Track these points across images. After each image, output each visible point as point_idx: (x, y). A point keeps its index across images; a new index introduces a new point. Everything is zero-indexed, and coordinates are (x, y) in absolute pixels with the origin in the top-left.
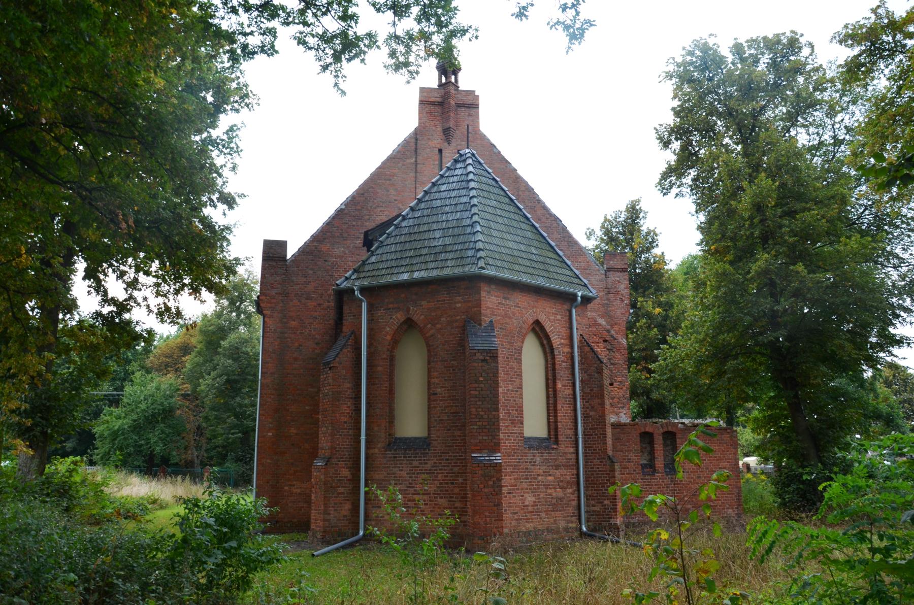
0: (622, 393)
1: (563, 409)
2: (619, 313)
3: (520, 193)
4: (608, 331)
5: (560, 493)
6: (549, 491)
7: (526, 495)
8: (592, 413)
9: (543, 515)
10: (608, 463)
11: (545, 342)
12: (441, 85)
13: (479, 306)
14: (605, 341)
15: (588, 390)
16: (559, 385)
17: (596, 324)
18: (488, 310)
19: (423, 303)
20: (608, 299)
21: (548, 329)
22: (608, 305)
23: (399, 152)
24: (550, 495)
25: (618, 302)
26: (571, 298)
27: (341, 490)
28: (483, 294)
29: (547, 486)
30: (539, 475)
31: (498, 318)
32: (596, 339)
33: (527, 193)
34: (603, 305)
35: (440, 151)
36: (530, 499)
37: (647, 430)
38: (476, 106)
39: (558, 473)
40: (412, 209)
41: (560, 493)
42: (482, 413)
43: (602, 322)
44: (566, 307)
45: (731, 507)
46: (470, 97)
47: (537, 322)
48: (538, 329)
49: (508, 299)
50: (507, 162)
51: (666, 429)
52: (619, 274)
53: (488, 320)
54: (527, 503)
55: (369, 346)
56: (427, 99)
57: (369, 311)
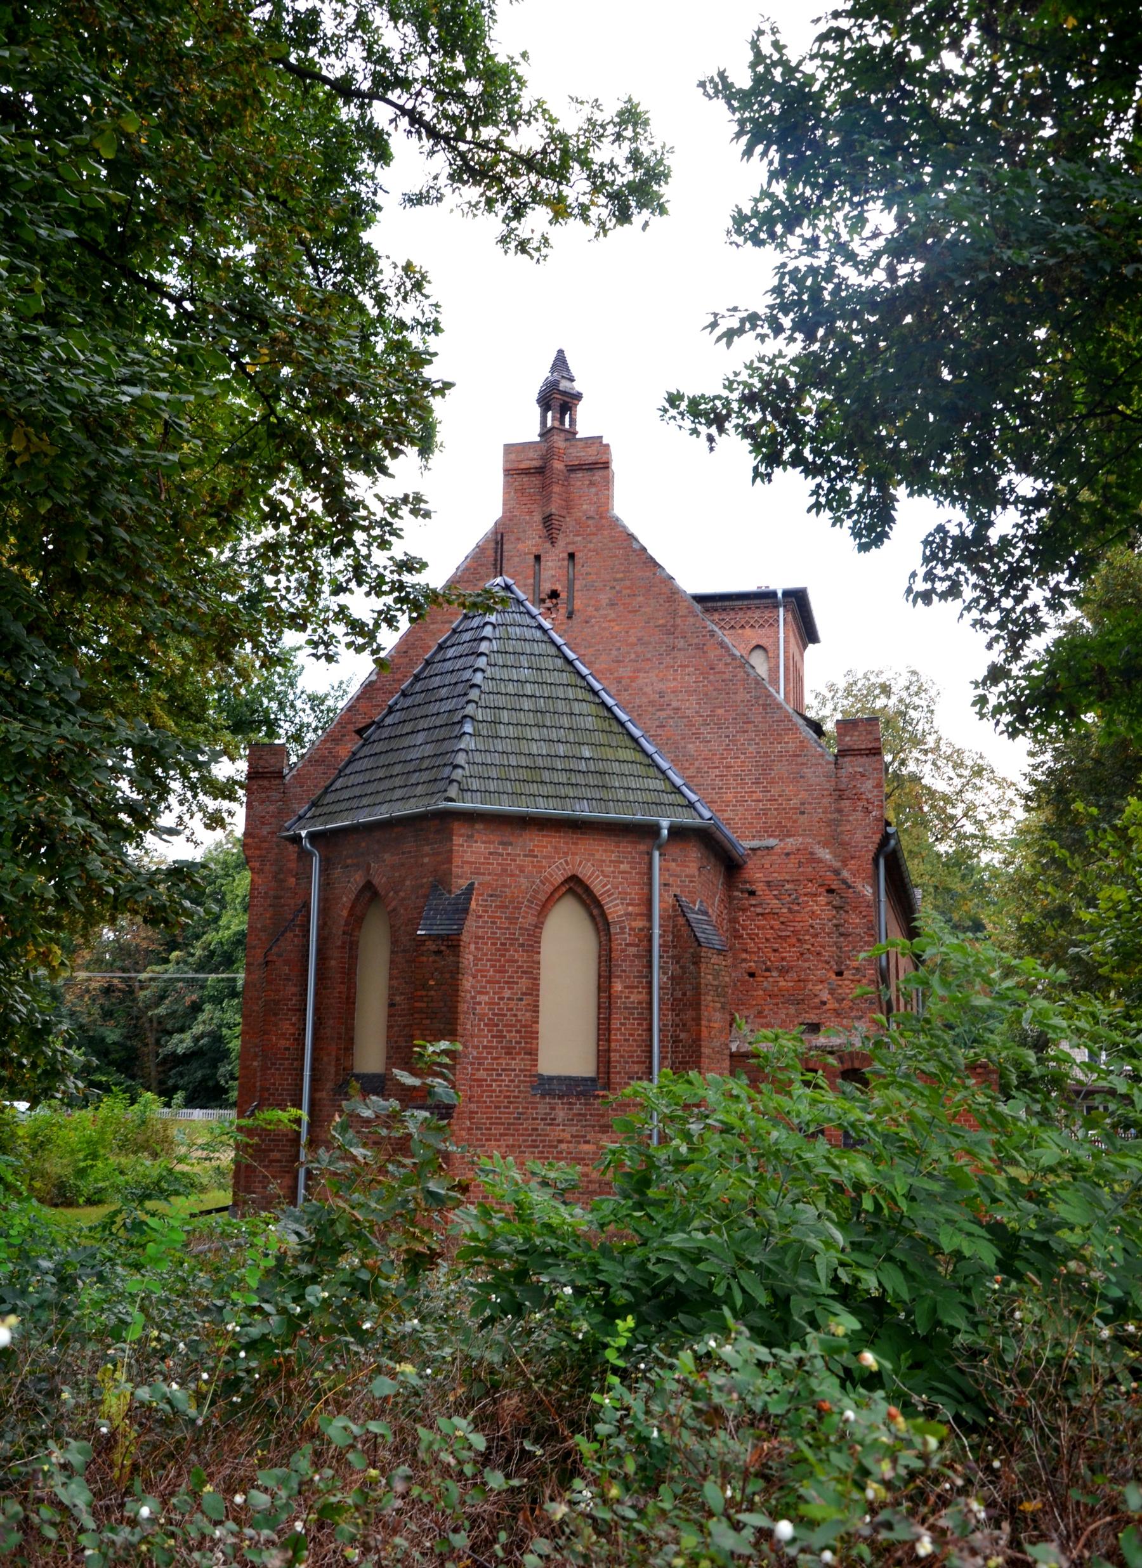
1: (623, 1028)
2: (859, 835)
3: (679, 621)
4: (837, 872)
8: (683, 1036)
11: (595, 912)
12: (545, 433)
13: (449, 861)
14: (830, 891)
15: (679, 994)
16: (618, 986)
17: (813, 859)
18: (467, 868)
19: (387, 856)
20: (840, 811)
21: (597, 889)
22: (837, 823)
23: (467, 569)
25: (859, 815)
26: (652, 830)
27: (276, 1155)
28: (457, 840)
31: (487, 878)
33: (692, 620)
35: (538, 558)
38: (606, 465)
40: (404, 694)
43: (825, 854)
44: (642, 847)
46: (593, 450)
47: (574, 879)
48: (576, 888)
50: (656, 565)
52: (864, 759)
53: (464, 883)
55: (320, 928)
57: (324, 871)
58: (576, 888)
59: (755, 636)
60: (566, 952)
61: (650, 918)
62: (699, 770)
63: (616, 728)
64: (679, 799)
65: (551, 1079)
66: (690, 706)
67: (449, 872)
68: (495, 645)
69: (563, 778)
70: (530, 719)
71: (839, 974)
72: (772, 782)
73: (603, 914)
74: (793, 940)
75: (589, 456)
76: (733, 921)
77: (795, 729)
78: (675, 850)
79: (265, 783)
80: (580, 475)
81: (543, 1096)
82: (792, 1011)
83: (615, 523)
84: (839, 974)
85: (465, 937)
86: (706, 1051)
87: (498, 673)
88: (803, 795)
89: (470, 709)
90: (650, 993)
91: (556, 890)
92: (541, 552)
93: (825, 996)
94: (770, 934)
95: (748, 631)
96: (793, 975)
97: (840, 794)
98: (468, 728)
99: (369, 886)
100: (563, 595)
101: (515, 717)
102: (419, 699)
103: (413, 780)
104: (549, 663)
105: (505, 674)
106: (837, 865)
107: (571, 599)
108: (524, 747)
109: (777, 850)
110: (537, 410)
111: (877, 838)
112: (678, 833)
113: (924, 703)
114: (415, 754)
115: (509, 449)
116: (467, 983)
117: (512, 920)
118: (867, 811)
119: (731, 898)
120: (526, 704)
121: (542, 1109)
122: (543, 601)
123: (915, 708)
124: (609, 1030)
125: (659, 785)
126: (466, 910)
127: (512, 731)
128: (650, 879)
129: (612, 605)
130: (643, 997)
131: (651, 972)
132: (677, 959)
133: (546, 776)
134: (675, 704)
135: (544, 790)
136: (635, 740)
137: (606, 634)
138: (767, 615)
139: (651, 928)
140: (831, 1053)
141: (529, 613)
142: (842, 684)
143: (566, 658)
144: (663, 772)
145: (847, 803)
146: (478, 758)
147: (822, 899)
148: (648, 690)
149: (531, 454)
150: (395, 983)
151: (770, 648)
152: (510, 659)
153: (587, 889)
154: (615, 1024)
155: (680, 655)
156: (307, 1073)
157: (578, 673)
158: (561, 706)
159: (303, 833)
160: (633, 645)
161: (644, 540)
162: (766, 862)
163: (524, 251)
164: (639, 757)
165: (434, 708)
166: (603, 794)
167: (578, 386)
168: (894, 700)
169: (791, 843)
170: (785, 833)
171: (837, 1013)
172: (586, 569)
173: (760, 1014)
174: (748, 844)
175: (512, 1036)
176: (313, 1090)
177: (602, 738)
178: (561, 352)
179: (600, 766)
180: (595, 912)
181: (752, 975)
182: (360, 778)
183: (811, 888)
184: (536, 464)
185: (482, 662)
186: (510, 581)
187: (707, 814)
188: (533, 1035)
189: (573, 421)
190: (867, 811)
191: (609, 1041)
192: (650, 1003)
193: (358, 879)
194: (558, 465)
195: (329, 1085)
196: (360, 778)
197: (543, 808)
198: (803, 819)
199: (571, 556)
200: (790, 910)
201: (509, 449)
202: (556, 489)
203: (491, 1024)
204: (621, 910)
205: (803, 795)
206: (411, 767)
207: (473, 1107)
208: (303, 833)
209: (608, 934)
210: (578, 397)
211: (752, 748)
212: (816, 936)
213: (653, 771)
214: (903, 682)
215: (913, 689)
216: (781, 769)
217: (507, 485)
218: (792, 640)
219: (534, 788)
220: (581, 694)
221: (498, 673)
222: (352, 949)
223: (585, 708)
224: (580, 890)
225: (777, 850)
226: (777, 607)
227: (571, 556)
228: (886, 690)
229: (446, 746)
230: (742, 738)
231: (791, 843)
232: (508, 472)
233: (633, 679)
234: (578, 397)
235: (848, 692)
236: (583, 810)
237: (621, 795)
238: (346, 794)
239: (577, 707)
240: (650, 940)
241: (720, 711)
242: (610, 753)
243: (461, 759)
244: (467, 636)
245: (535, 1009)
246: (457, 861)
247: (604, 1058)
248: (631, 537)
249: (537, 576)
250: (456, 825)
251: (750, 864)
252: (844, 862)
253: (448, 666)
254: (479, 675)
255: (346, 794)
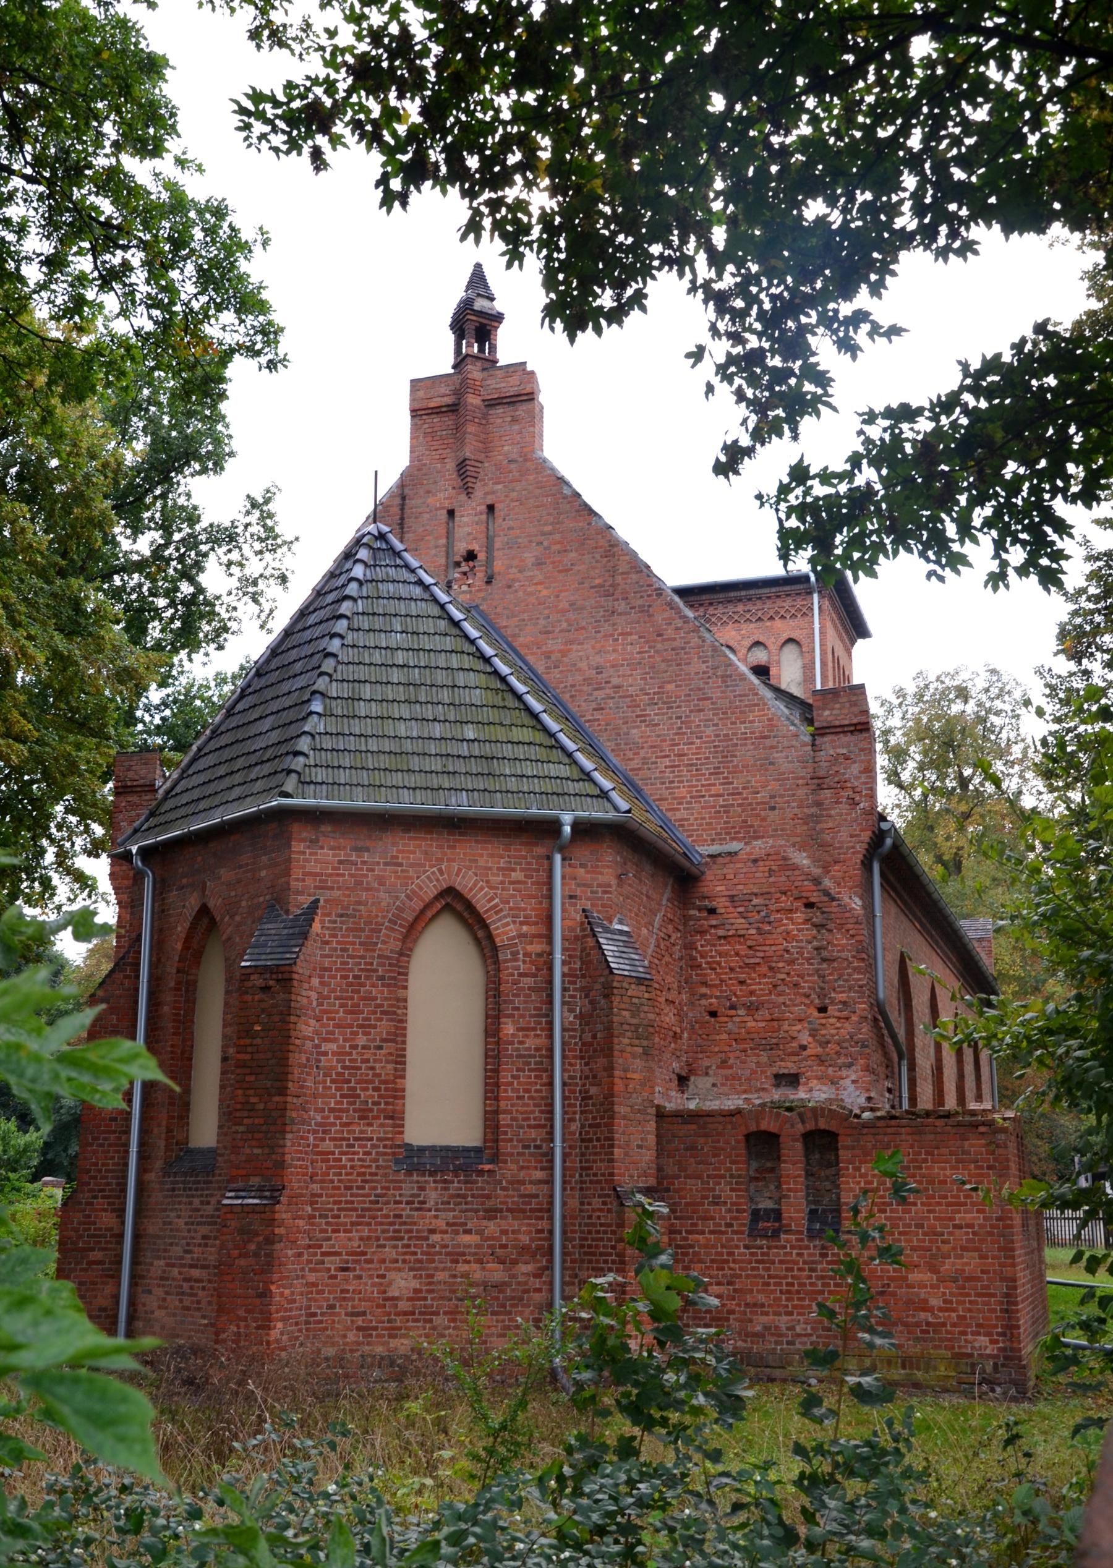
0: (848, 1028)
2: (843, 835)
3: (619, 579)
4: (817, 881)
5: (497, 1273)
6: (462, 1268)
7: (391, 1275)
8: (593, 1090)
9: (441, 1320)
10: (614, 1206)
12: (460, 362)
13: (287, 873)
14: (809, 905)
15: (588, 1037)
17: (788, 866)
18: (309, 881)
19: (222, 871)
20: (818, 804)
21: (482, 905)
22: (816, 819)
24: (466, 1275)
25: (844, 807)
26: (551, 827)
28: (297, 846)
29: (456, 1257)
30: (432, 1231)
31: (337, 893)
32: (786, 902)
33: (634, 577)
34: (806, 819)
35: (451, 513)
36: (402, 1283)
37: (764, 1126)
39: (492, 1227)
41: (497, 1273)
42: (253, 1100)
43: (802, 859)
44: (540, 850)
45: (982, 1328)
46: (515, 380)
48: (455, 904)
49: (368, 850)
50: (591, 512)
51: (810, 1126)
53: (305, 900)
54: (393, 1292)
56: (424, 405)
58: (455, 904)
59: (785, 628)
60: (442, 985)
61: (549, 939)
62: (645, 760)
63: (511, 702)
64: (589, 788)
65: (422, 1149)
66: (634, 682)
67: (287, 887)
68: (360, 606)
69: (436, 765)
70: (401, 693)
71: (823, 1010)
72: (735, 771)
73: (490, 937)
74: (764, 969)
75: (511, 387)
76: (689, 946)
77: (762, 703)
78: (583, 852)
79: (134, 799)
80: (500, 410)
81: (409, 1173)
82: (764, 1059)
83: (543, 466)
84: (823, 1010)
85: (301, 968)
86: (621, 1109)
87: (361, 639)
88: (773, 786)
89: (321, 684)
90: (551, 1037)
91: (427, 906)
92: (455, 505)
93: (805, 1038)
94: (735, 962)
95: (778, 623)
96: (764, 1013)
97: (819, 783)
98: (317, 706)
99: (204, 911)
100: (482, 556)
101: (379, 692)
102: (273, 677)
103: (253, 776)
104: (428, 626)
105: (371, 640)
106: (817, 871)
107: (490, 560)
108: (389, 728)
109: (742, 856)
110: (450, 338)
111: (866, 836)
112: (585, 830)
113: (1008, 707)
114: (260, 743)
115: (415, 384)
116: (307, 1028)
117: (369, 946)
118: (854, 803)
119: (686, 919)
120: (396, 676)
121: (408, 1189)
122: (458, 564)
123: (998, 713)
124: (497, 1085)
125: (564, 771)
126: (305, 935)
127: (374, 709)
128: (551, 890)
129: (539, 564)
130: (542, 1041)
131: (552, 1010)
132: (586, 991)
133: (415, 763)
134: (615, 681)
135: (412, 780)
136: (535, 716)
137: (533, 600)
138: (799, 603)
139: (551, 953)
140: (789, 1109)
141: (406, 566)
142: (911, 689)
143: (450, 619)
144: (570, 755)
145: (828, 793)
146: (327, 742)
147: (799, 916)
148: (583, 665)
149: (444, 390)
150: (229, 1030)
151: (804, 642)
152: (378, 623)
153: (470, 906)
154: (506, 1077)
155: (620, 620)
156: (134, 1149)
157: (466, 636)
158: (441, 677)
159: (134, 849)
160: (563, 611)
161: (578, 484)
162: (729, 871)
163: (282, 44)
164: (539, 737)
165: (285, 687)
166: (489, 783)
167: (499, 306)
168: (972, 703)
169: (759, 846)
170: (751, 834)
171: (821, 1060)
172: (505, 525)
173: (724, 1064)
174: (705, 850)
175: (368, 1095)
176: (141, 1170)
177: (493, 715)
178: (478, 266)
179: (487, 749)
180: (480, 934)
181: (713, 1014)
182: (202, 778)
183: (786, 902)
184: (448, 400)
185: (341, 626)
186: (385, 529)
187: (624, 805)
188: (398, 1094)
189: (493, 348)
190: (854, 803)
191: (497, 1099)
192: (551, 1050)
193: (193, 903)
194: (473, 400)
195: (159, 1164)
196: (202, 778)
197: (406, 802)
198: (773, 815)
199: (491, 508)
200: (760, 932)
201: (415, 384)
202: (471, 428)
203: (340, 1080)
204: (512, 930)
205: (773, 786)
206: (253, 759)
207: (316, 1188)
208: (134, 849)
209: (497, 962)
210: (499, 318)
211: (710, 731)
212: (791, 962)
213: (556, 754)
214: (981, 684)
215: (994, 691)
216: (746, 754)
217: (415, 428)
218: (831, 632)
219: (397, 779)
220: (467, 662)
221: (361, 639)
222: (188, 989)
223: (472, 679)
224: (459, 907)
225: (742, 856)
226: (810, 593)
227: (491, 508)
228: (963, 694)
229: (292, 731)
230: (696, 719)
231: (759, 846)
232: (415, 413)
233: (564, 653)
234: (499, 318)
235: (919, 697)
236: (461, 804)
237: (512, 784)
238: (185, 798)
239: (461, 678)
240: (551, 969)
241: (670, 687)
242: (501, 733)
243: (304, 744)
244: (330, 598)
245: (400, 1060)
246: (296, 873)
247: (491, 1121)
248: (562, 481)
249: (449, 535)
250: (295, 828)
251: (709, 875)
252: (826, 869)
253: (307, 635)
254: (337, 642)
255: (185, 798)
